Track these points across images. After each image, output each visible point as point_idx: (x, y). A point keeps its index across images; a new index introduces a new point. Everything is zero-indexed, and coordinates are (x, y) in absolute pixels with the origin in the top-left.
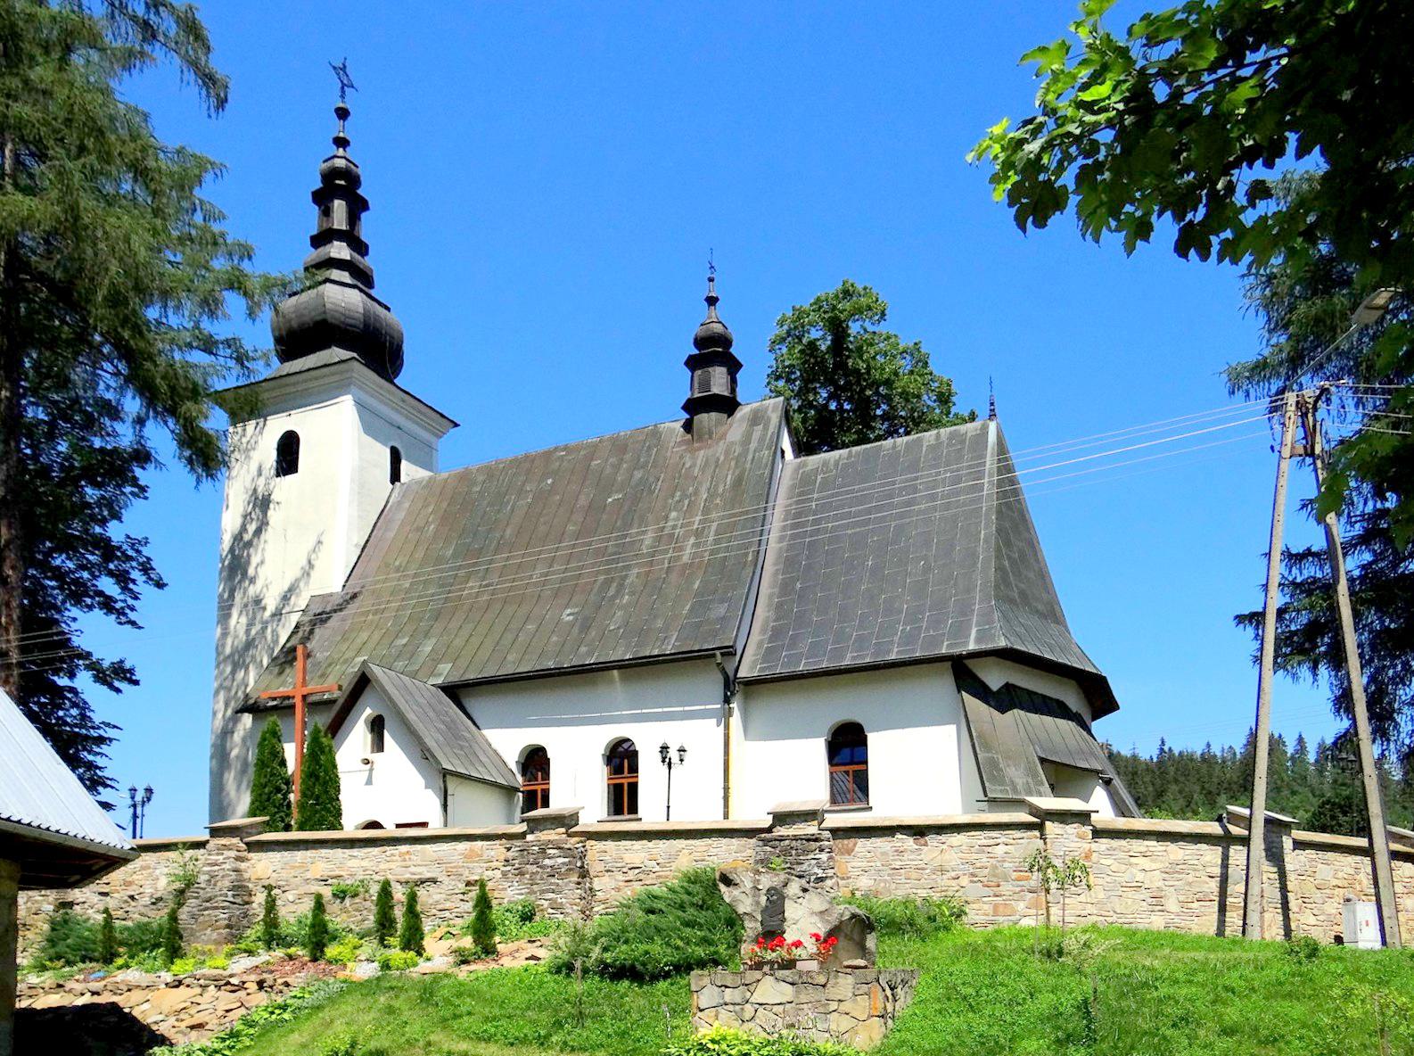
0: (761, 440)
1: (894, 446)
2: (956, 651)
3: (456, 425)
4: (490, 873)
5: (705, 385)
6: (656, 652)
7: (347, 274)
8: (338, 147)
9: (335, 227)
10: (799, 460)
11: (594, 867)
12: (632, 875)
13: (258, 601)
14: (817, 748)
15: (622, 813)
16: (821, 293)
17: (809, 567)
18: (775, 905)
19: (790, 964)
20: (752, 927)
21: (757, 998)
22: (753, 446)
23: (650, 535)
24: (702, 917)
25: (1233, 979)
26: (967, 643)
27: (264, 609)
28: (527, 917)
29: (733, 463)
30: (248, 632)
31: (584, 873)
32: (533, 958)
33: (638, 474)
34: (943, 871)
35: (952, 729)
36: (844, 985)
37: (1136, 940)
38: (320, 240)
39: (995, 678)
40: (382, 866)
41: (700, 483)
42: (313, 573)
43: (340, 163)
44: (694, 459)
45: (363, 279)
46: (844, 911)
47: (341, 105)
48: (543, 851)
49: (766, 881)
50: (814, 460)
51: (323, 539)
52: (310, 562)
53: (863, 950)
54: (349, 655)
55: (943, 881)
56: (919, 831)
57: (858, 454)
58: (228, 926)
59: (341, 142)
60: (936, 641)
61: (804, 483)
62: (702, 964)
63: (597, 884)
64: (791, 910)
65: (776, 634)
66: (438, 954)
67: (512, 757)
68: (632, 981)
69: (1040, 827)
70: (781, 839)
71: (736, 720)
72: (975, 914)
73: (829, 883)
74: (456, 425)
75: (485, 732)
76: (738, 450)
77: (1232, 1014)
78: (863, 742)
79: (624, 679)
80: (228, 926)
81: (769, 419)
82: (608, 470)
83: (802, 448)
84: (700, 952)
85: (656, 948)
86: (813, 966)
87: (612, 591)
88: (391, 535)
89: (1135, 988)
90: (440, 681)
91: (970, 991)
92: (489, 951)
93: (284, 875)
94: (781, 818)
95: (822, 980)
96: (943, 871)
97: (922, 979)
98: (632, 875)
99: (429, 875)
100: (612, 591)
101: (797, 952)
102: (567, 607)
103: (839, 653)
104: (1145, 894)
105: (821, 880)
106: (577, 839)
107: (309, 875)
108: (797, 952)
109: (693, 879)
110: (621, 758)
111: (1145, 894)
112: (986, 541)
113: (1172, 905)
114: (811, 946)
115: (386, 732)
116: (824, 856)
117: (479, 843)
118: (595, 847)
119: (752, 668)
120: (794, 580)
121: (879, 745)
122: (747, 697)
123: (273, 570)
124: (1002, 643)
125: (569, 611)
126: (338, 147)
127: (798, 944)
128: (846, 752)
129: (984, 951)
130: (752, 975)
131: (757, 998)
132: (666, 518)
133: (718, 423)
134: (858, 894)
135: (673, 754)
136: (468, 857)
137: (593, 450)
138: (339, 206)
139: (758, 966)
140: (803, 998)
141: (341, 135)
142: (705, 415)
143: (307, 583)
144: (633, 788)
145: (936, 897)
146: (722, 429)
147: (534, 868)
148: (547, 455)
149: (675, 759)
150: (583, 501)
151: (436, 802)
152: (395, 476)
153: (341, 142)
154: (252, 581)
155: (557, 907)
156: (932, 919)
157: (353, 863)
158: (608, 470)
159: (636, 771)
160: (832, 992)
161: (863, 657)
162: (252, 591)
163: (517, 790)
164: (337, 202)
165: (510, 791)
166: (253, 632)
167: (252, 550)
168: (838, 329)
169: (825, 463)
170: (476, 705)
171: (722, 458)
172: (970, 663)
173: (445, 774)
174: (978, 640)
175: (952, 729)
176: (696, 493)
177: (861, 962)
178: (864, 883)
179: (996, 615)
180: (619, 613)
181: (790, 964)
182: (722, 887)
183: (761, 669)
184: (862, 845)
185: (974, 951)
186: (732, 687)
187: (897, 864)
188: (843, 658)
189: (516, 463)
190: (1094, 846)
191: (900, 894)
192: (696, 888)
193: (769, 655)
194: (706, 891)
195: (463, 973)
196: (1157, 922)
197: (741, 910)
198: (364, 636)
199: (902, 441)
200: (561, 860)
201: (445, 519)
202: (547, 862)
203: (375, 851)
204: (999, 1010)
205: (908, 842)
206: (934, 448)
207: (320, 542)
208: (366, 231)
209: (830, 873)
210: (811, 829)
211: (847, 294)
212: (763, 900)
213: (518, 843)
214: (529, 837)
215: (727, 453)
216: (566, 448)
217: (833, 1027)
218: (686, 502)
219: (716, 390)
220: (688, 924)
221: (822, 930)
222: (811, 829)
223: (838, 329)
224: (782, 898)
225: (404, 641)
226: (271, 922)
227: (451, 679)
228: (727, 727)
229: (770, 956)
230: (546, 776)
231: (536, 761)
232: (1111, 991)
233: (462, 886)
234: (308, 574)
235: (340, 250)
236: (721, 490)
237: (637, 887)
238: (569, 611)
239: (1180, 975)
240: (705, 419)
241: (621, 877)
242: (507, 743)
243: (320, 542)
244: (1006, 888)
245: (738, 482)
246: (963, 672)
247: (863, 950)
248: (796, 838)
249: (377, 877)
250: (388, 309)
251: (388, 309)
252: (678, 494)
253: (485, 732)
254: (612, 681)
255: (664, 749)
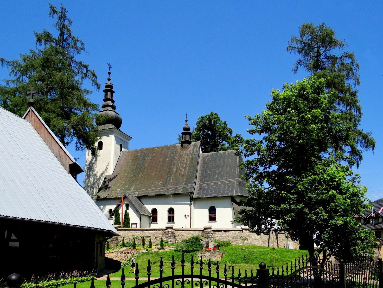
0: (196, 150)
1: (221, 153)
2: (231, 195)
3: (132, 138)
4: (159, 236)
5: (185, 138)
6: (178, 193)
7: (111, 108)
8: (109, 80)
9: (109, 98)
10: (203, 154)
11: (176, 235)
12: (182, 236)
13: (95, 175)
14: (207, 211)
15: (171, 221)
16: (207, 114)
17: (205, 176)
18: (208, 243)
19: (210, 251)
20: (205, 246)
21: (206, 255)
22: (195, 151)
23: (175, 168)
24: (195, 244)
25: (263, 253)
26: (233, 194)
27: (97, 177)
28: (166, 243)
29: (191, 154)
30: (94, 181)
31: (175, 236)
32: (170, 249)
33: (172, 155)
34: (229, 237)
35: (231, 208)
36: (217, 253)
37: (255, 247)
38: (105, 100)
39: (238, 200)
40: (141, 234)
41: (185, 158)
42: (108, 170)
43: (109, 84)
44: (183, 152)
45: (114, 108)
46: (217, 244)
47: (109, 72)
48: (169, 233)
49: (206, 240)
50: (206, 154)
51: (109, 163)
52: (107, 168)
53: (219, 249)
54: (116, 188)
55: (229, 238)
56: (225, 231)
57: (214, 154)
58: (116, 243)
59: (109, 80)
60: (228, 193)
61: (204, 158)
62: (196, 250)
63: (177, 238)
64: (210, 244)
65: (200, 190)
66: (154, 249)
67: (150, 211)
68: (187, 253)
69: (242, 231)
70: (205, 232)
71: (192, 205)
72: (234, 243)
73: (212, 238)
74: (132, 138)
75: (145, 205)
76: (192, 152)
77: (262, 257)
78: (215, 210)
79: (173, 197)
80: (116, 243)
81: (197, 146)
82: (166, 153)
83: (203, 152)
84: (196, 249)
85: (190, 248)
86: (213, 251)
87: (168, 179)
88: (122, 163)
89: (251, 254)
90: (136, 195)
91: (232, 254)
92: (163, 248)
93: (124, 235)
94: (205, 229)
95: (214, 253)
96: (229, 237)
97: (226, 253)
98: (182, 236)
99: (149, 236)
100: (168, 179)
101: (211, 249)
102: (160, 182)
103: (211, 194)
104: (257, 240)
105: (211, 238)
106: (174, 231)
107: (128, 235)
108: (211, 249)
109: (193, 238)
110: (171, 211)
111: (257, 240)
112: (237, 174)
113: (261, 242)
114: (212, 249)
115: (129, 207)
116: (212, 234)
117: (158, 231)
118: (176, 232)
119: (196, 196)
120: (203, 179)
121: (218, 210)
122: (194, 201)
123: (99, 169)
124: (239, 194)
125: (160, 183)
126: (109, 80)
127: (211, 248)
128: (212, 211)
129: (234, 249)
130: (205, 252)
131: (206, 255)
132: (178, 165)
133: (188, 146)
134: (216, 240)
135: (187, 216)
136: (156, 233)
137: (163, 148)
138: (109, 93)
139: (206, 251)
140: (211, 255)
141: (109, 78)
142: (185, 144)
143: (106, 172)
144: (173, 217)
145: (228, 241)
146: (189, 147)
147: (167, 235)
148: (153, 148)
149: (187, 217)
150: (161, 159)
151: (139, 220)
152: (121, 150)
153: (109, 80)
154: (94, 171)
155: (171, 241)
156: (227, 244)
157: (136, 233)
158: (166, 153)
159: (174, 214)
160: (215, 254)
161: (216, 195)
162: (94, 173)
163: (151, 216)
164: (109, 93)
165: (150, 217)
166: (95, 181)
167: (94, 165)
168: (210, 121)
169: (208, 155)
170: (143, 200)
171: (189, 153)
172: (234, 197)
173: (141, 215)
174: (235, 193)
175: (231, 208)
176: (184, 160)
177: (219, 251)
178: (217, 238)
179: (238, 189)
180: (170, 184)
181: (210, 251)
182: (201, 241)
183: (197, 196)
184: (217, 233)
185: (232, 249)
186: (192, 199)
187: (222, 236)
188: (212, 195)
189: (147, 149)
190: (250, 234)
191: (222, 240)
192: (194, 239)
193: (198, 193)
194: (196, 240)
195: (160, 251)
196: (259, 244)
197: (203, 244)
198: (119, 185)
199: (222, 152)
200: (171, 234)
201: (133, 160)
202: (169, 234)
203: (140, 232)
204: (235, 256)
205: (224, 232)
206: (228, 154)
207: (109, 164)
208: (114, 99)
209: (212, 237)
210: (210, 230)
211: (212, 114)
212: (206, 242)
213: (164, 231)
214: (166, 230)
215: (190, 152)
216: (157, 147)
217: (215, 258)
218: (182, 162)
219: (187, 140)
220: (193, 245)
221: (214, 246)
222: (210, 230)
223: (210, 121)
224: (209, 242)
225: (127, 186)
226: (123, 243)
227: (138, 195)
228: (191, 207)
229: (208, 250)
230: (157, 214)
231: (155, 211)
232: (241, 255)
233: (155, 237)
234: (107, 170)
235: (110, 103)
236: (189, 160)
237: (183, 238)
238: (160, 183)
239: (257, 253)
240: (185, 145)
241: (180, 237)
242: (149, 208)
243: (109, 164)
244: (238, 239)
245: (192, 159)
246: (233, 199)
247: (219, 249)
248: (208, 232)
249: (140, 236)
250: (119, 114)
251: (119, 114)
252: (180, 160)
253: (145, 205)
254: (171, 197)
255: (185, 216)
